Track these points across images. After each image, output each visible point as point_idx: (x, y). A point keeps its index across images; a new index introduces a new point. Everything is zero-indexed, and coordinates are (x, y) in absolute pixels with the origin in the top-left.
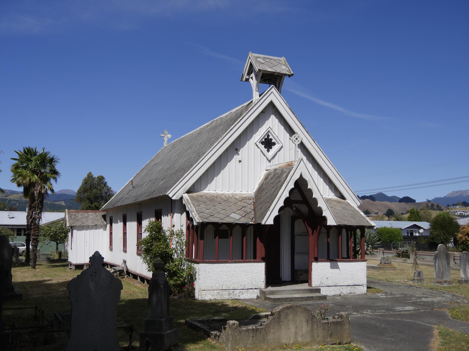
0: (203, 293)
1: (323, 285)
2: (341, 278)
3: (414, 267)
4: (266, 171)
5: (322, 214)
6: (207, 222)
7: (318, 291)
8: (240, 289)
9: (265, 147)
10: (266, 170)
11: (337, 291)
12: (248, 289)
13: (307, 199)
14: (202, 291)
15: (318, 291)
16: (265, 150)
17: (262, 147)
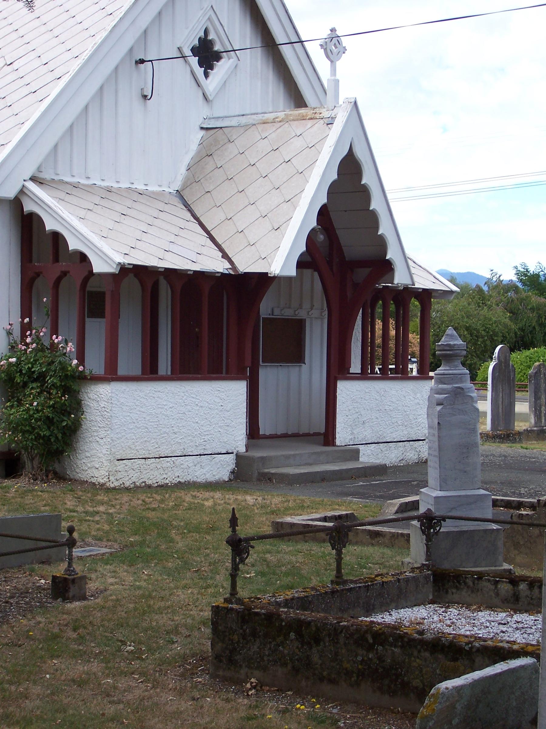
0: (119, 468)
1: (356, 440)
2: (387, 423)
3: (98, 439)
4: (203, 133)
5: (385, 255)
6: (165, 268)
7: (354, 454)
8: (197, 453)
9: (201, 64)
10: (202, 128)
11: (380, 455)
12: (211, 454)
13: (331, 213)
14: (117, 463)
15: (354, 454)
16: (200, 71)
17: (194, 61)
